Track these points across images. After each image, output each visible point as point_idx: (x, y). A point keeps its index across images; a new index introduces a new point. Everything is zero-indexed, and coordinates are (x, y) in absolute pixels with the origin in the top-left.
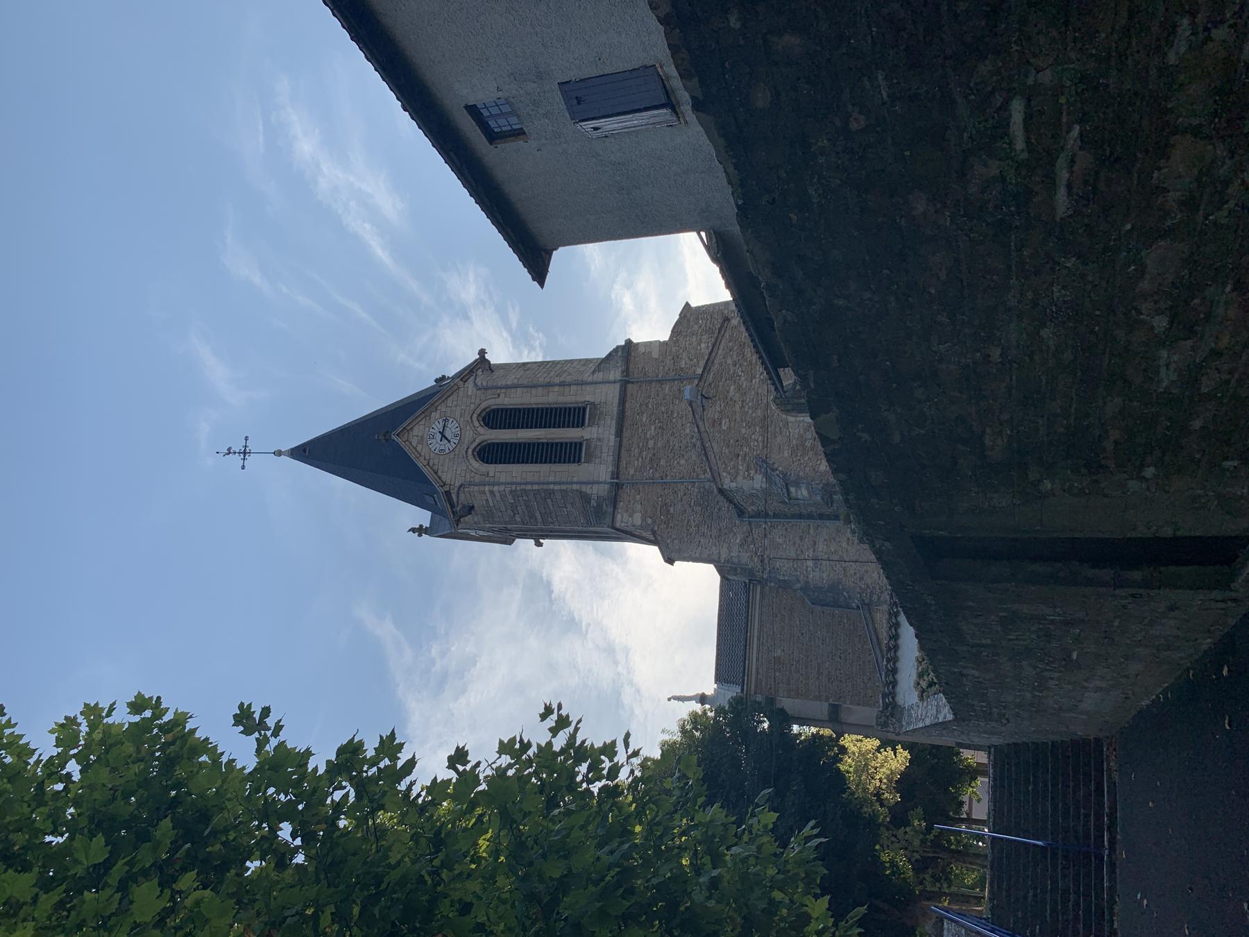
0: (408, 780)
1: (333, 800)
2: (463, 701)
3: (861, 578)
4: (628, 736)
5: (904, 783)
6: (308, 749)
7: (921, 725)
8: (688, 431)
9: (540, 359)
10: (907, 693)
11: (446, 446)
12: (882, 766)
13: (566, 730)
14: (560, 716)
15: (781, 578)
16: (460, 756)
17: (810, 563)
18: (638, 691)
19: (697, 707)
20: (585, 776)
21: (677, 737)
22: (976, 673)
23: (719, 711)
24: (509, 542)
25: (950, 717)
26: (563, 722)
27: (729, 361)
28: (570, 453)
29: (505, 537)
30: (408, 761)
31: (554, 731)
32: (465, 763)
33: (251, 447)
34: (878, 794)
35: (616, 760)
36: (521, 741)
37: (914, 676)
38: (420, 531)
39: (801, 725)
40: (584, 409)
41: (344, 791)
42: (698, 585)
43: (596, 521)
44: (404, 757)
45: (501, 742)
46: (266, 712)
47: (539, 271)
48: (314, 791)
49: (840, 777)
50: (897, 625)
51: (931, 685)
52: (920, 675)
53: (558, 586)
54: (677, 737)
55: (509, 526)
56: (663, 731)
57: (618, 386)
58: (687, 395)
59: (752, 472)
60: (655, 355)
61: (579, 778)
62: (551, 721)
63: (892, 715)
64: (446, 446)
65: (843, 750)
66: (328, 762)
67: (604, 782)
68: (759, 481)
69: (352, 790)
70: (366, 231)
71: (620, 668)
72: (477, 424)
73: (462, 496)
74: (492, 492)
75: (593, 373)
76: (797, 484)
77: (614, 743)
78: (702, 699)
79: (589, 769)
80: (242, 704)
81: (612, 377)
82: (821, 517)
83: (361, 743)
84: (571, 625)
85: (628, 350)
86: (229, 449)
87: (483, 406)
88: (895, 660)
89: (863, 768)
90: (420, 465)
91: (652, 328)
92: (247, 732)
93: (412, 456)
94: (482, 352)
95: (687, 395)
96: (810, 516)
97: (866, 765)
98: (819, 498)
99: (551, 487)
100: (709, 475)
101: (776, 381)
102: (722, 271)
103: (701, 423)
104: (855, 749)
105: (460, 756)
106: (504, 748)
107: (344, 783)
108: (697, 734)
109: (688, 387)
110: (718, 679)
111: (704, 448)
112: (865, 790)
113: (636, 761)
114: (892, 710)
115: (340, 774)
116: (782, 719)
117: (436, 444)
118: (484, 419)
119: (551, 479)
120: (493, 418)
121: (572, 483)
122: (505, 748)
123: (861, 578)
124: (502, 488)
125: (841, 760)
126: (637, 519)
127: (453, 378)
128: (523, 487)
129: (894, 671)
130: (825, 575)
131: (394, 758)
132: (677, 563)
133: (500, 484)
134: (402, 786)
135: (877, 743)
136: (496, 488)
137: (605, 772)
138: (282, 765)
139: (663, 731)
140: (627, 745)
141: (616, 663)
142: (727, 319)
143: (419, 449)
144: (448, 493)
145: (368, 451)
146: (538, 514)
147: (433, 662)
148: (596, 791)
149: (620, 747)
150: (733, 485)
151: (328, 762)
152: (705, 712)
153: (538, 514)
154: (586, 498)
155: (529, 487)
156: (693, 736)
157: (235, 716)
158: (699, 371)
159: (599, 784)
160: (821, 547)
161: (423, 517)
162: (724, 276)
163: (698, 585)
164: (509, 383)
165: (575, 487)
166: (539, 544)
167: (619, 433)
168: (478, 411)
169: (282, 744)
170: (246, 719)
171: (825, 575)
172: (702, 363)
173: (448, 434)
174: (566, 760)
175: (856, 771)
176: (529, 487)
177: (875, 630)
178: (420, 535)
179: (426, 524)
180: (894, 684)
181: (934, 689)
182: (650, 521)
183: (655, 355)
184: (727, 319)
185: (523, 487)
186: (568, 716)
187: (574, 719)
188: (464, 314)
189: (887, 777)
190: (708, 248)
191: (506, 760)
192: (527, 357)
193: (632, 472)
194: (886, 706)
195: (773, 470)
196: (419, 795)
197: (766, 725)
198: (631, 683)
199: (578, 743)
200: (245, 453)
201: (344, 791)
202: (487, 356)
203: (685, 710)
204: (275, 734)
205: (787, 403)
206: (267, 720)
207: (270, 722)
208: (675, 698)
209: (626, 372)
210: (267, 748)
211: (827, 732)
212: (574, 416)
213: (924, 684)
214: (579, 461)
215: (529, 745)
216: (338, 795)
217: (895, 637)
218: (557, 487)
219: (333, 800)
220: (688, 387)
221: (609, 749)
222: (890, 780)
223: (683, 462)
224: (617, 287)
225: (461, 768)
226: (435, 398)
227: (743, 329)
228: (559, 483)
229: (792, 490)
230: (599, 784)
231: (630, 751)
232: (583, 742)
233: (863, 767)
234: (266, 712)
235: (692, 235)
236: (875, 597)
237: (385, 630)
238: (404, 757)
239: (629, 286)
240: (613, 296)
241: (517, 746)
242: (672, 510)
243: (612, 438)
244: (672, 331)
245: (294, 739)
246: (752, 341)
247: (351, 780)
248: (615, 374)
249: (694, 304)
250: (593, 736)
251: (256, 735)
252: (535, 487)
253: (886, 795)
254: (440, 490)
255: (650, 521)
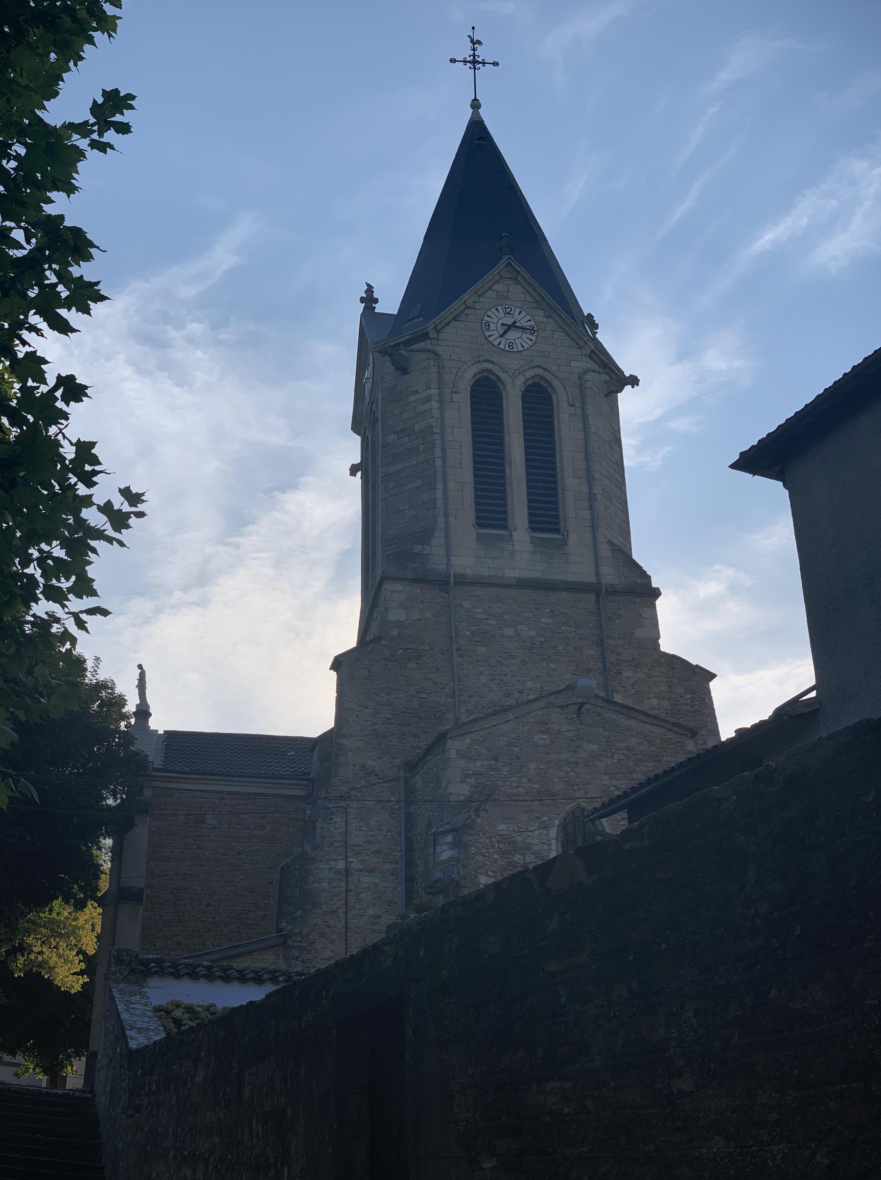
0: (43, 326)
1: (12, 229)
2: (128, 372)
3: (322, 935)
4: (105, 613)
5: (38, 984)
6: (76, 188)
7: (121, 1007)
8: (529, 685)
9: (626, 463)
10: (162, 992)
11: (494, 334)
12: (60, 956)
13: (108, 526)
14: (128, 515)
15: (318, 825)
16: (74, 390)
17: (341, 865)
18: (148, 621)
19: (131, 707)
20: (49, 555)
21: (89, 678)
22: (200, 1078)
23: (127, 737)
24: (357, 426)
25: (133, 1045)
26: (119, 520)
27: (634, 741)
28: (491, 513)
29: (362, 422)
30: (66, 322)
31: (107, 508)
32: (66, 400)
33: (482, 70)
34: (22, 949)
35: (71, 596)
36: (95, 473)
37: (188, 1001)
38: (369, 299)
39: (113, 850)
40: (557, 531)
41: (22, 241)
42: (304, 706)
43: (392, 553)
44: (70, 315)
45: (92, 444)
46: (124, 129)
47: (753, 461)
48: (22, 204)
49: (43, 900)
50: (258, 980)
51: (178, 1022)
52: (190, 1009)
53: (292, 500)
54: (89, 678)
55: (379, 425)
56: (97, 659)
57: (592, 579)
58: (582, 682)
59: (472, 781)
60: (639, 633)
61: (43, 546)
62: (120, 503)
63: (133, 971)
64: (494, 334)
65: (80, 906)
66: (61, 218)
67: (41, 580)
68: (459, 790)
69: (25, 252)
70: (798, 219)
71: (178, 594)
72: (529, 374)
73: (423, 356)
74: (429, 399)
75: (610, 543)
76: (457, 844)
77: (94, 593)
78: (143, 713)
79: (57, 560)
80: (133, 97)
81: (604, 570)
82: (410, 879)
83: (88, 257)
84: (237, 522)
85: (646, 593)
86: (479, 42)
87: (556, 383)
88: (210, 977)
89: (57, 931)
90: (465, 296)
91: (680, 628)
92: (96, 109)
93: (478, 285)
94: (634, 381)
95: (582, 682)
96: (410, 863)
97: (61, 935)
98: (438, 875)
99: (440, 486)
100: (465, 718)
101: (609, 808)
102: (762, 723)
103: (542, 704)
104: (81, 922)
105: (74, 390)
106: (85, 449)
107: (34, 241)
108: (95, 707)
109: (594, 684)
110: (171, 735)
111: (506, 710)
112: (28, 932)
113: (71, 625)
114: (141, 971)
115: (46, 233)
116: (119, 825)
117: (497, 318)
118: (535, 384)
119: (451, 485)
120: (538, 399)
121: (446, 516)
122: (85, 450)
123: (322, 935)
124: (436, 413)
125: (67, 902)
126: (396, 615)
127: (596, 340)
128: (438, 444)
129: (194, 975)
130: (325, 885)
131: (68, 304)
132: (334, 674)
133: (441, 409)
134: (34, 319)
135: (91, 951)
136: (435, 405)
137: (54, 582)
138: (55, 161)
139: (97, 659)
140: (91, 612)
141: (185, 589)
142: (693, 734)
143: (490, 294)
144: (425, 336)
145: (483, 217)
146: (398, 467)
147: (179, 326)
148: (29, 571)
149: (88, 602)
150: (452, 754)
151: (61, 218)
152: (125, 717)
153: (398, 467)
154: (425, 536)
155: (438, 452)
156: (94, 702)
157: (116, 91)
158: (618, 698)
159: (38, 574)
160: (366, 880)
161: (390, 303)
162: (755, 726)
163: (304, 706)
164: (591, 420)
165: (441, 520)
166: (353, 470)
167: (522, 584)
168: (547, 376)
169: (80, 154)
170: (112, 107)
171: (325, 885)
172: (629, 702)
173: (512, 335)
174: (68, 527)
175: (52, 921)
176: (438, 452)
177: (251, 952)
178: (362, 300)
179: (379, 308)
180: (177, 975)
181: (171, 1026)
182: (394, 633)
183: (639, 633)
184: (693, 734)
185: (438, 444)
186: (128, 527)
187: (124, 535)
188: (685, 352)
189: (45, 962)
190: (795, 702)
191: (69, 452)
192: (627, 441)
193: (467, 604)
194: (145, 963)
195: (477, 810)
196: (24, 343)
197: (110, 802)
198: (158, 611)
199: (93, 543)
200: (474, 62)
201: (22, 241)
202: (628, 388)
203: (126, 689)
204: (94, 145)
205: (576, 825)
206: (112, 132)
207: (110, 136)
208: (142, 676)
209: (614, 592)
210: (75, 137)
211: (104, 884)
212: (546, 516)
213: (177, 1013)
214: (480, 525)
215: (90, 484)
216: (18, 235)
217: (242, 978)
218: (439, 494)
219: (12, 229)
220: (594, 684)
221: (85, 587)
222: (40, 965)
223: (484, 679)
224: (730, 572)
225: (58, 394)
226: (564, 315)
227: (682, 758)
228: (445, 497)
229: (449, 838)
230: (38, 574)
231: (84, 616)
232: (94, 551)
233: (57, 932)
234: (124, 129)
235: (810, 679)
236: (296, 953)
237: (223, 257)
238: (70, 315)
239: (734, 590)
240: (717, 567)
241: (88, 468)
242: (412, 665)
243: (516, 574)
244: (674, 656)
245: (91, 170)
246: (666, 773)
247: (38, 249)
248: (610, 575)
249: (712, 685)
250: (103, 563)
251: (92, 120)
252: (438, 463)
253: (21, 960)
254: (430, 326)
255: (394, 633)
